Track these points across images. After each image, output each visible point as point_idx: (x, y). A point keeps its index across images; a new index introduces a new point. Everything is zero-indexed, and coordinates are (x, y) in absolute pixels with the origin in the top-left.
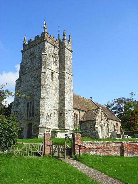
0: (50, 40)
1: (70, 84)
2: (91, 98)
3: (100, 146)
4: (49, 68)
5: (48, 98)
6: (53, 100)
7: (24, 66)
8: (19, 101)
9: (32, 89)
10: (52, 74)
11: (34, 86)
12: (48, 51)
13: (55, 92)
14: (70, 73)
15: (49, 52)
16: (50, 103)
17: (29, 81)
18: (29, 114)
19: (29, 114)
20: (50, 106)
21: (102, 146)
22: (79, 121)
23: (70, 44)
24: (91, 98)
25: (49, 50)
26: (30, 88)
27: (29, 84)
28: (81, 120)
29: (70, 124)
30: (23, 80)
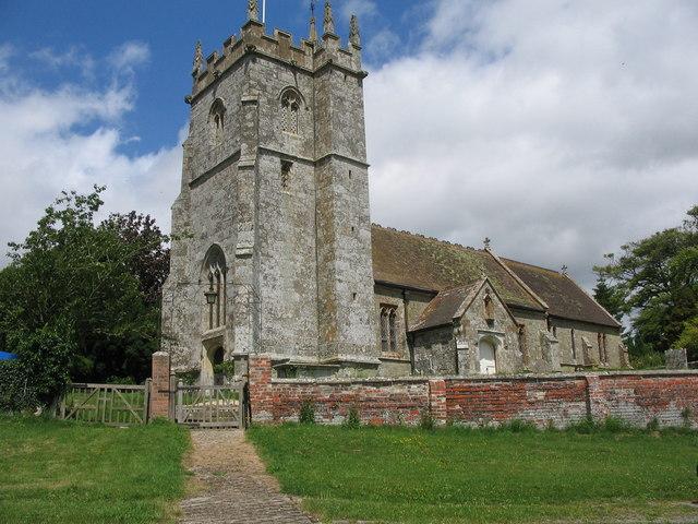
0: (274, 46)
1: (357, 196)
2: (487, 241)
3: (344, 392)
4: (271, 147)
5: (271, 252)
6: (293, 259)
7: (197, 151)
8: (187, 273)
9: (219, 228)
10: (286, 167)
11: (224, 217)
12: (265, 86)
13: (298, 230)
14: (354, 158)
15: (269, 89)
16: (277, 271)
17: (211, 200)
18: (215, 317)
19: (215, 317)
20: (278, 283)
21: (350, 393)
22: (403, 331)
23: (352, 50)
24: (487, 241)
25: (269, 85)
26: (213, 224)
27: (211, 210)
28: (412, 328)
29: (359, 343)
30: (194, 200)
